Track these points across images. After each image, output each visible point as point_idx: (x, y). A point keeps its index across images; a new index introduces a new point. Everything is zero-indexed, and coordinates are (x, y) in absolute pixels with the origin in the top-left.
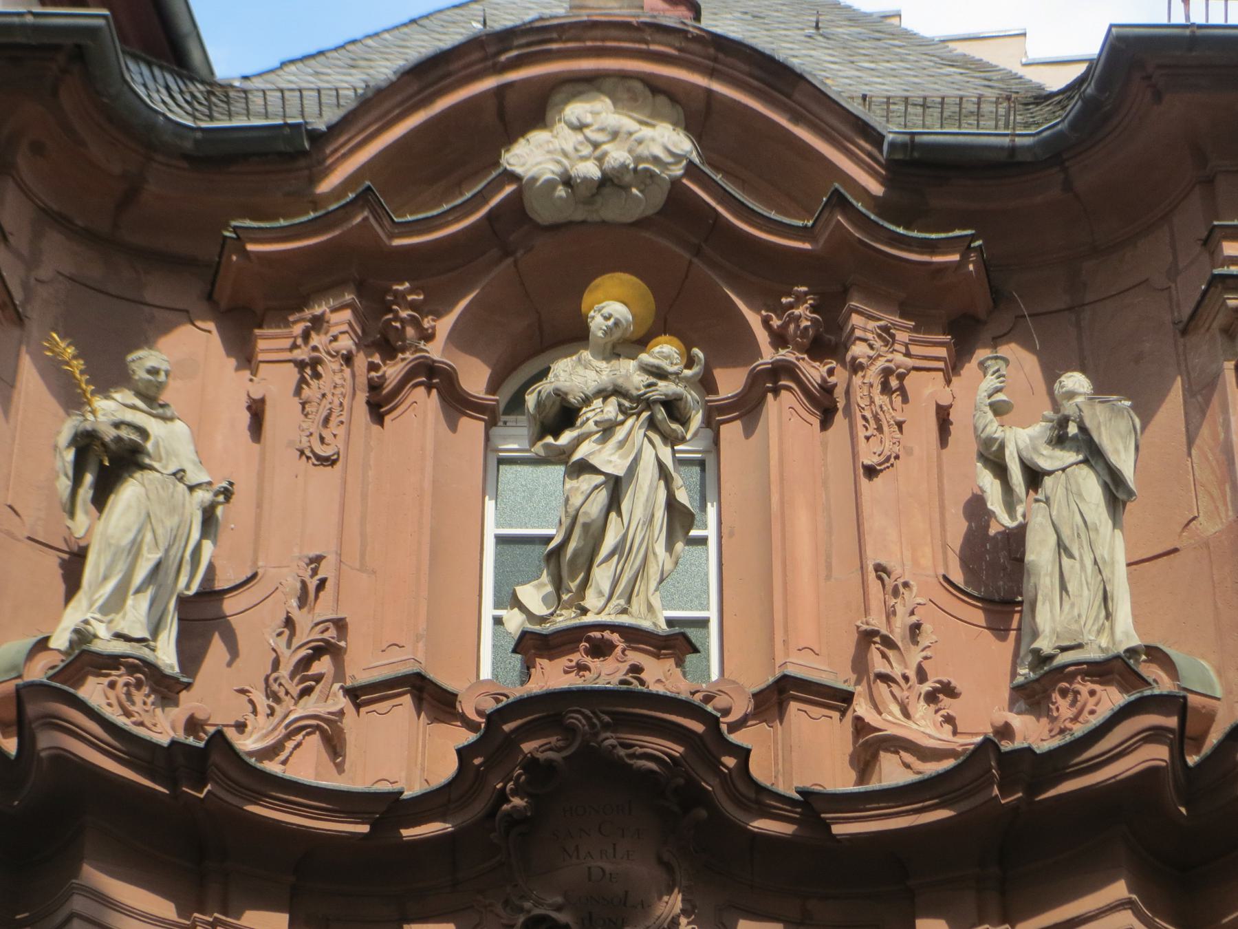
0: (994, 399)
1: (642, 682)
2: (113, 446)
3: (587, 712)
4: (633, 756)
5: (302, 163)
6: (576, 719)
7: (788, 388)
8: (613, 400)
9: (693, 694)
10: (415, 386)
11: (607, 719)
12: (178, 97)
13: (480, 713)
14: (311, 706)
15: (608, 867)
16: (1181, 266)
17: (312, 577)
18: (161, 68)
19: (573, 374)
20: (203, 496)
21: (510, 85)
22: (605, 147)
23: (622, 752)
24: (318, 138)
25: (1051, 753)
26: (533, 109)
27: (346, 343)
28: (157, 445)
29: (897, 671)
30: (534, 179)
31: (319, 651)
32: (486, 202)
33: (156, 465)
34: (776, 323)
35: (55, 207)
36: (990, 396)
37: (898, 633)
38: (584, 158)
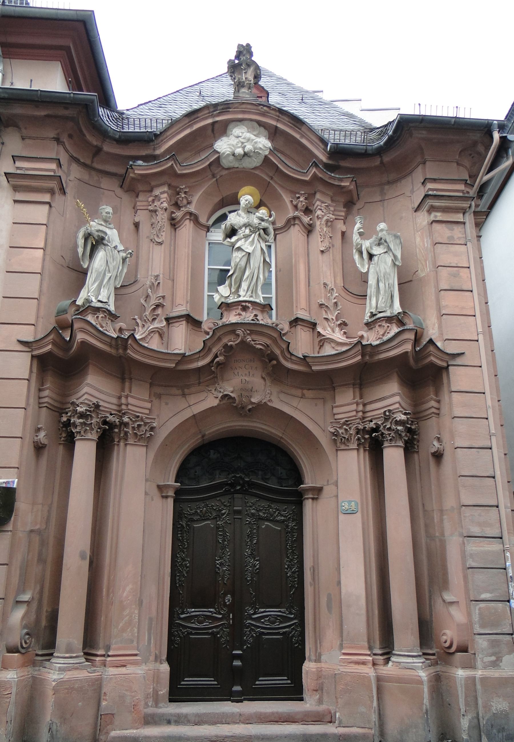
0: (359, 231)
1: (258, 320)
2: (96, 238)
3: (243, 330)
4: (256, 344)
5: (151, 144)
6: (239, 332)
7: (298, 224)
9: (273, 324)
10: (186, 219)
11: (248, 332)
12: (110, 118)
13: (210, 329)
14: (156, 325)
15: (247, 379)
16: (415, 190)
17: (155, 282)
18: (106, 109)
19: (235, 219)
21: (217, 122)
22: (245, 144)
23: (253, 343)
24: (156, 136)
25: (377, 346)
26: (220, 129)
27: (165, 205)
28: (109, 237)
29: (330, 317)
30: (224, 153)
31: (158, 306)
32: (208, 160)
33: (109, 244)
34: (295, 203)
35: (75, 156)
36: (358, 230)
37: (331, 305)
38: (239, 147)
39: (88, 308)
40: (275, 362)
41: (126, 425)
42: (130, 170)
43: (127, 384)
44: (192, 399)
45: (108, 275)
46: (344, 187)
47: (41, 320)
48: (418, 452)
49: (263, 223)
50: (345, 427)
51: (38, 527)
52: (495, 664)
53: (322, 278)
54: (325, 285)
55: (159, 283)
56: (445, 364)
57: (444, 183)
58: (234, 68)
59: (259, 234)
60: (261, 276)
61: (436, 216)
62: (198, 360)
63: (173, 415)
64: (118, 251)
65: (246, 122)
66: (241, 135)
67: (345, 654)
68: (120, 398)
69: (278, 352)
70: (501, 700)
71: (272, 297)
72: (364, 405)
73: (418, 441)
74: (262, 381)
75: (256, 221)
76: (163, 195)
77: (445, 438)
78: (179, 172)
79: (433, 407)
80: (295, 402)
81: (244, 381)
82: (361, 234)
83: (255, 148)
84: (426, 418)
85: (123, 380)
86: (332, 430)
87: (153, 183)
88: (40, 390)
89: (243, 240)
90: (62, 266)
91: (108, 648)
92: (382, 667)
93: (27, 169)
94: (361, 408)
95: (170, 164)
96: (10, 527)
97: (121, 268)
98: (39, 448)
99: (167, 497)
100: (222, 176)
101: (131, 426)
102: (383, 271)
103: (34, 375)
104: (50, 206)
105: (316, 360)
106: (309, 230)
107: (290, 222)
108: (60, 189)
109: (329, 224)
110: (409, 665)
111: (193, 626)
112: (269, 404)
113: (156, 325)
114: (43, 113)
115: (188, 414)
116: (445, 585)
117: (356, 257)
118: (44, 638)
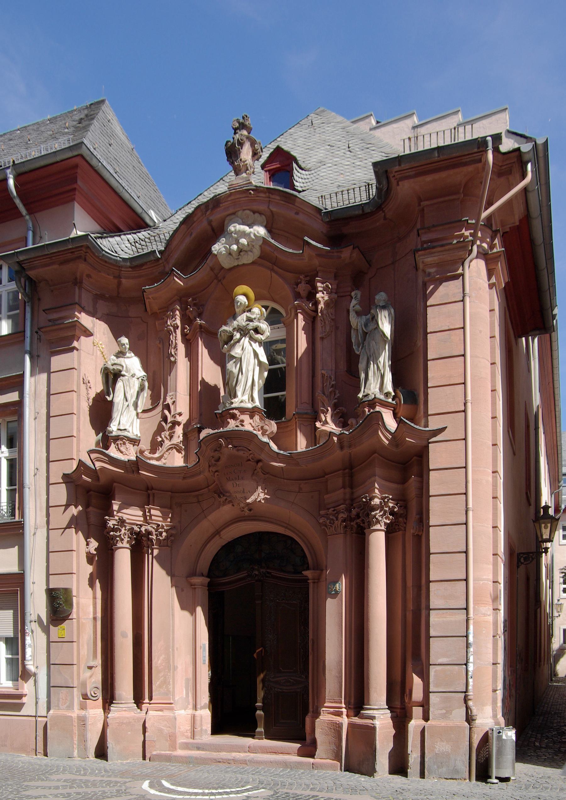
26: (218, 231)
52: (444, 716)
70: (444, 743)
71: (370, 771)
118: (109, 697)
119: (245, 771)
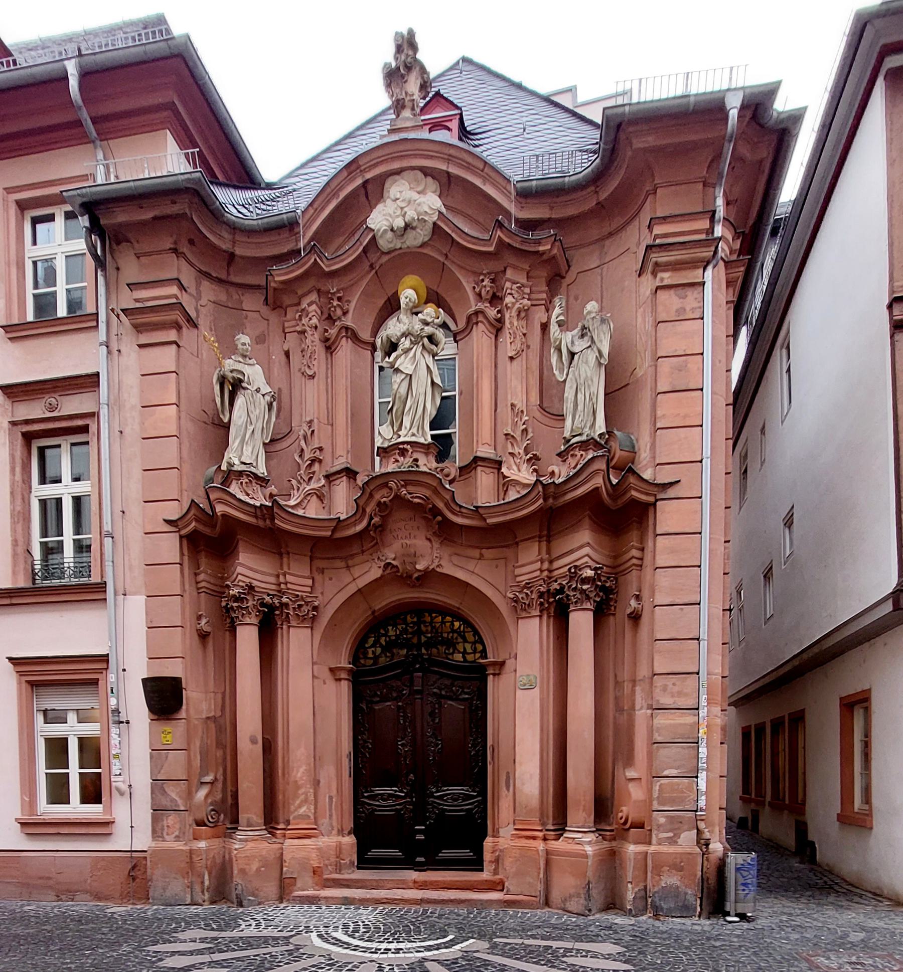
1: (418, 466)
6: (392, 484)
7: (481, 322)
8: (408, 338)
14: (314, 485)
15: (408, 542)
19: (394, 327)
20: (268, 398)
23: (409, 496)
26: (371, 192)
27: (315, 321)
29: (516, 450)
32: (361, 244)
33: (249, 387)
38: (398, 216)
39: (230, 475)
40: (439, 518)
41: (286, 605)
42: (270, 278)
43: (285, 560)
44: (356, 572)
45: (251, 428)
46: (544, 253)
47: (185, 493)
48: (614, 615)
49: (426, 328)
50: (525, 590)
51: (212, 714)
52: (673, 841)
53: (509, 396)
54: (513, 405)
55: (313, 431)
56: (651, 499)
57: (678, 222)
58: (393, 77)
59: (423, 344)
60: (429, 405)
61: (662, 280)
62: (355, 524)
63: (339, 588)
64: (263, 395)
65: (405, 174)
66: (398, 196)
67: (516, 829)
68: (278, 576)
69: (441, 505)
72: (551, 562)
73: (616, 602)
74: (428, 543)
75: (418, 326)
76: (311, 305)
77: (645, 594)
78: (327, 269)
79: (633, 557)
80: (471, 566)
81: (405, 545)
82: (560, 324)
83: (418, 215)
84: (625, 572)
85: (281, 555)
86: (512, 596)
87: (300, 292)
88: (196, 574)
89: (403, 357)
90: (205, 423)
91: (288, 822)
92: (553, 842)
93: (148, 299)
94: (546, 565)
95: (312, 260)
96: (183, 714)
97: (266, 417)
98: (203, 636)
99: (340, 680)
100: (382, 265)
101: (291, 607)
102: (583, 376)
103: (186, 558)
104: (179, 346)
105: (492, 510)
106: (498, 327)
107: (472, 320)
108: (188, 321)
109: (523, 314)
110: (583, 841)
111: (377, 803)
112: (438, 570)
113: (314, 485)
114: (148, 215)
115: (352, 589)
116: (629, 761)
117: (554, 359)
119: (469, 960)
